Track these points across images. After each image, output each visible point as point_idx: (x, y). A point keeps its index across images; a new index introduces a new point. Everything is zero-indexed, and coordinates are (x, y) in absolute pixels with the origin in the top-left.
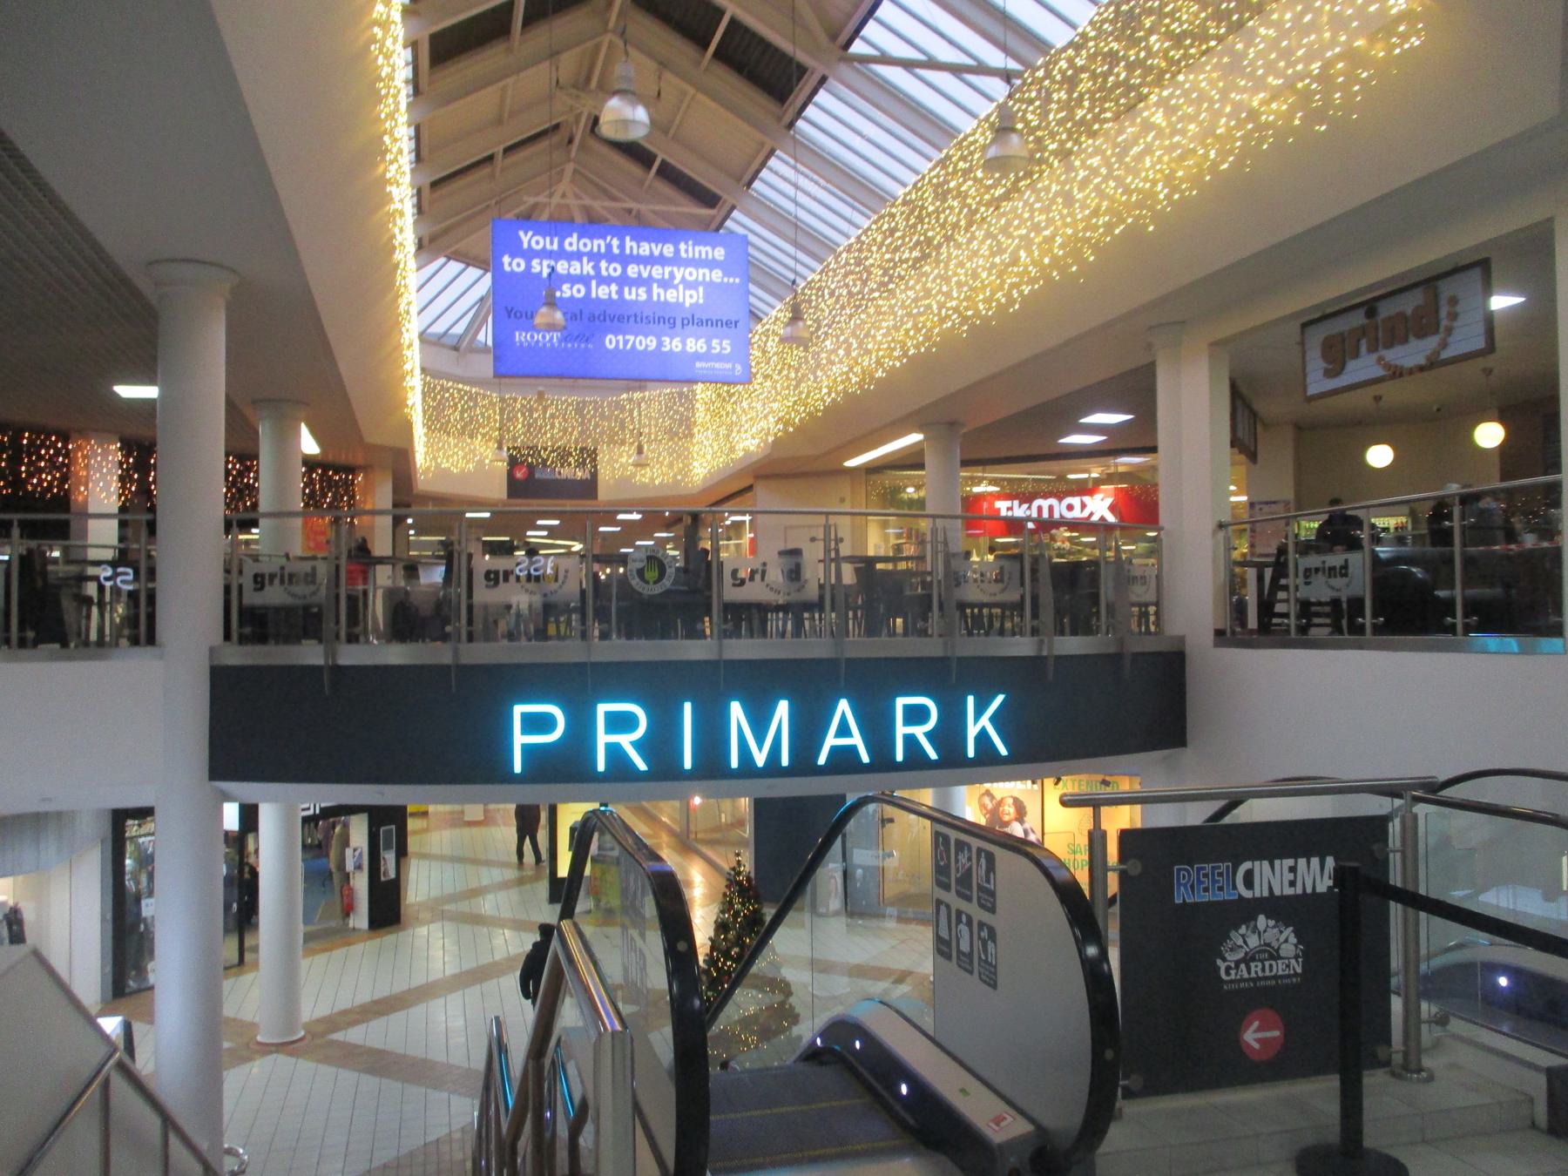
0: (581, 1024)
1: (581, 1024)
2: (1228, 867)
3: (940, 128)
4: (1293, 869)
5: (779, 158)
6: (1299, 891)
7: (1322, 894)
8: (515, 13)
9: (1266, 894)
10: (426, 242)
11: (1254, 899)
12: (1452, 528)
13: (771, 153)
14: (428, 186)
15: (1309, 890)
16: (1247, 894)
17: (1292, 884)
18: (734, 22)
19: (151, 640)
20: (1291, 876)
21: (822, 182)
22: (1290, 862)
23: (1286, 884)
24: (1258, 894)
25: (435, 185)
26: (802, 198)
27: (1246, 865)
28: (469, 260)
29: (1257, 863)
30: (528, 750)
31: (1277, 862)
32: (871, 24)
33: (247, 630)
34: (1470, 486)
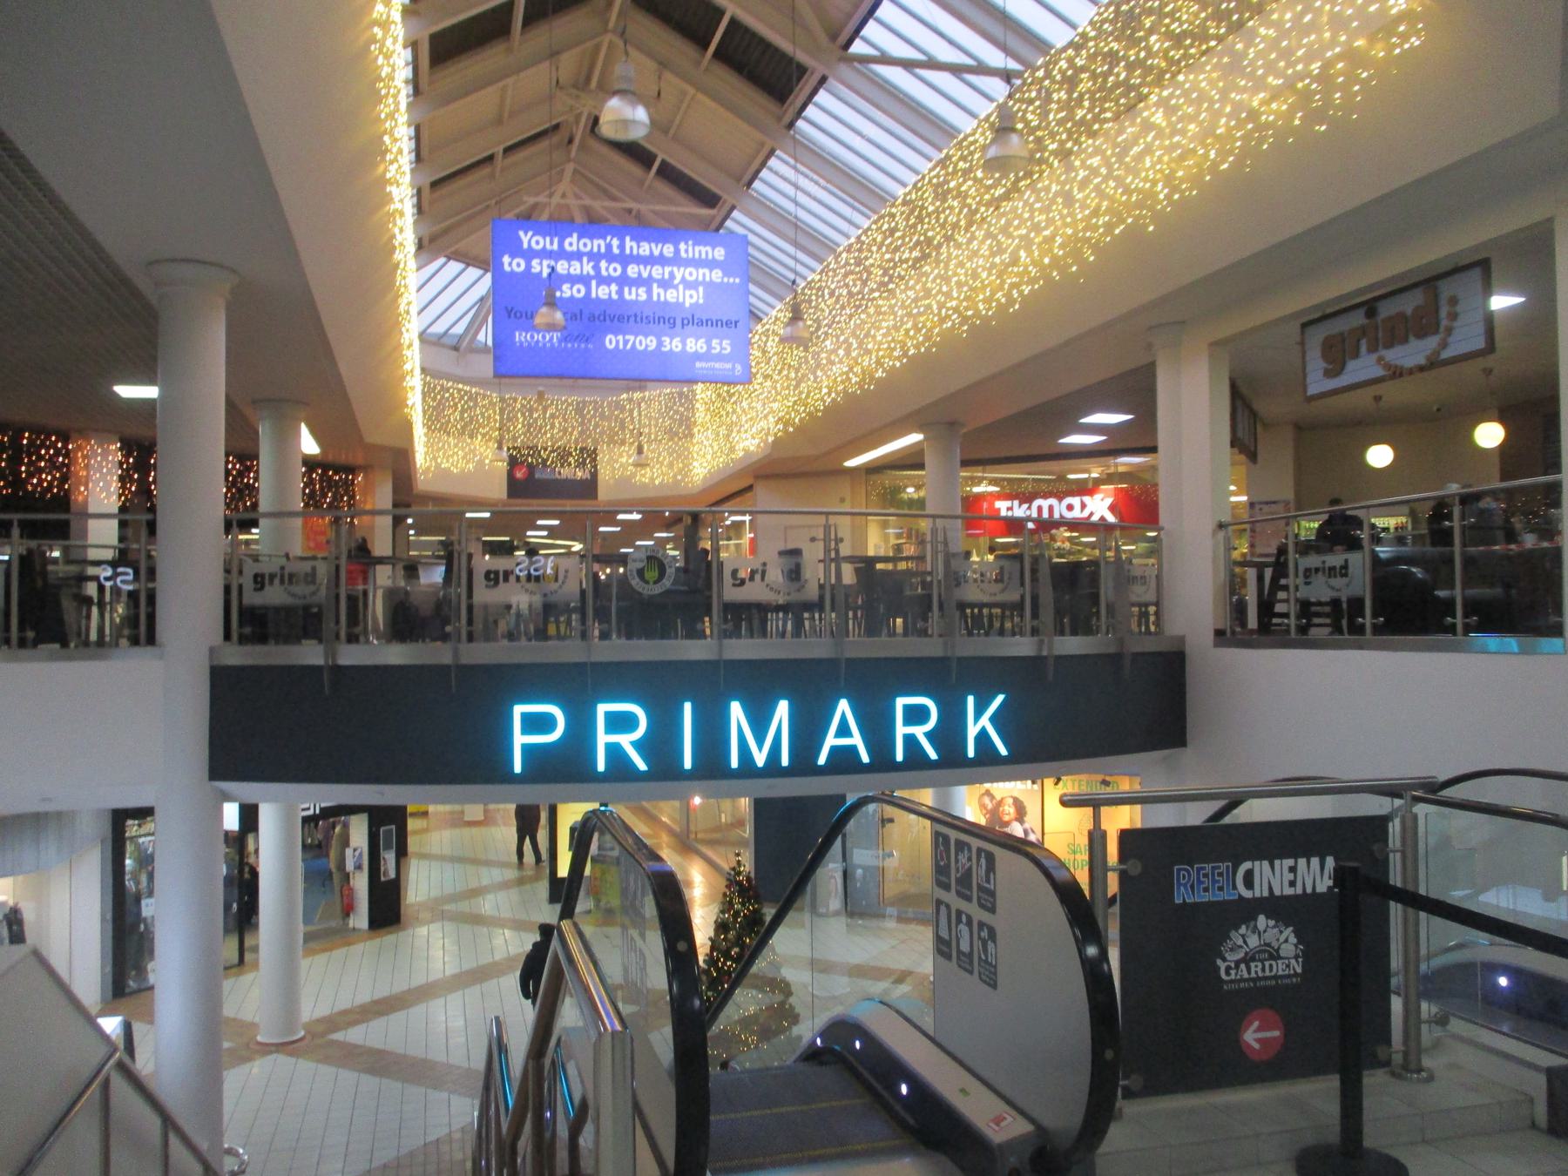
0: (581, 1024)
1: (581, 1024)
2: (1228, 867)
3: (940, 128)
4: (1293, 869)
5: (779, 158)
6: (1299, 891)
8: (515, 13)
9: (1266, 894)
10: (426, 242)
12: (1452, 528)
13: (771, 153)
14: (428, 186)
15: (1309, 890)
16: (1247, 894)
17: (1292, 884)
18: (734, 22)
20: (1291, 876)
22: (1290, 862)
23: (1286, 884)
24: (1258, 894)
25: (435, 185)
26: (802, 198)
27: (1246, 865)
28: (469, 260)
29: (1257, 863)
30: (528, 750)
32: (871, 24)
34: (1470, 486)
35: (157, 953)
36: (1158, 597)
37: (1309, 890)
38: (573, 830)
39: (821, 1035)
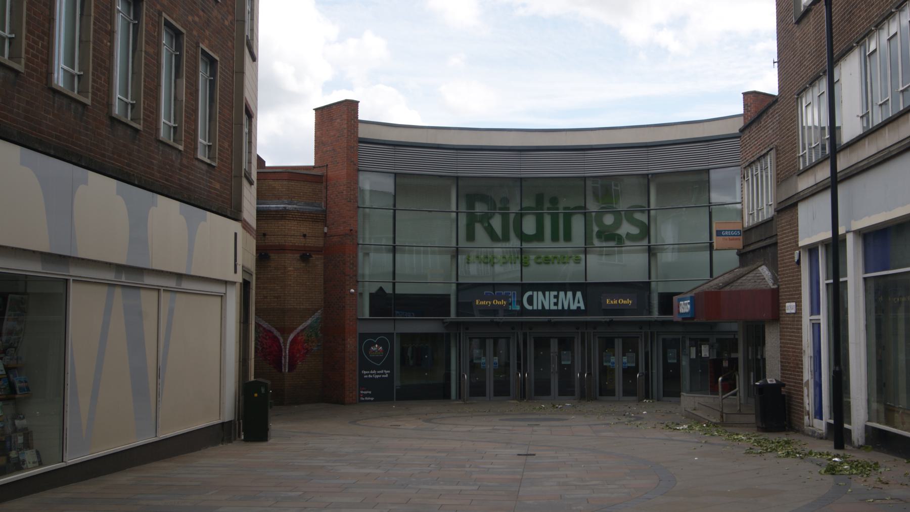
2: (514, 293)
3: (460, 383)
6: (560, 307)
7: (548, 291)
9: (540, 308)
11: (533, 310)
15: (566, 307)
16: (530, 308)
17: (556, 304)
19: (27, 428)
20: (555, 300)
21: (246, 130)
22: (556, 293)
23: (552, 304)
24: (535, 308)
27: (529, 293)
29: (535, 293)
30: (132, 100)
31: (547, 293)
33: (29, 456)
35: (476, 239)
36: (30, 468)
37: (566, 307)
38: (65, 65)
39: (694, 302)
